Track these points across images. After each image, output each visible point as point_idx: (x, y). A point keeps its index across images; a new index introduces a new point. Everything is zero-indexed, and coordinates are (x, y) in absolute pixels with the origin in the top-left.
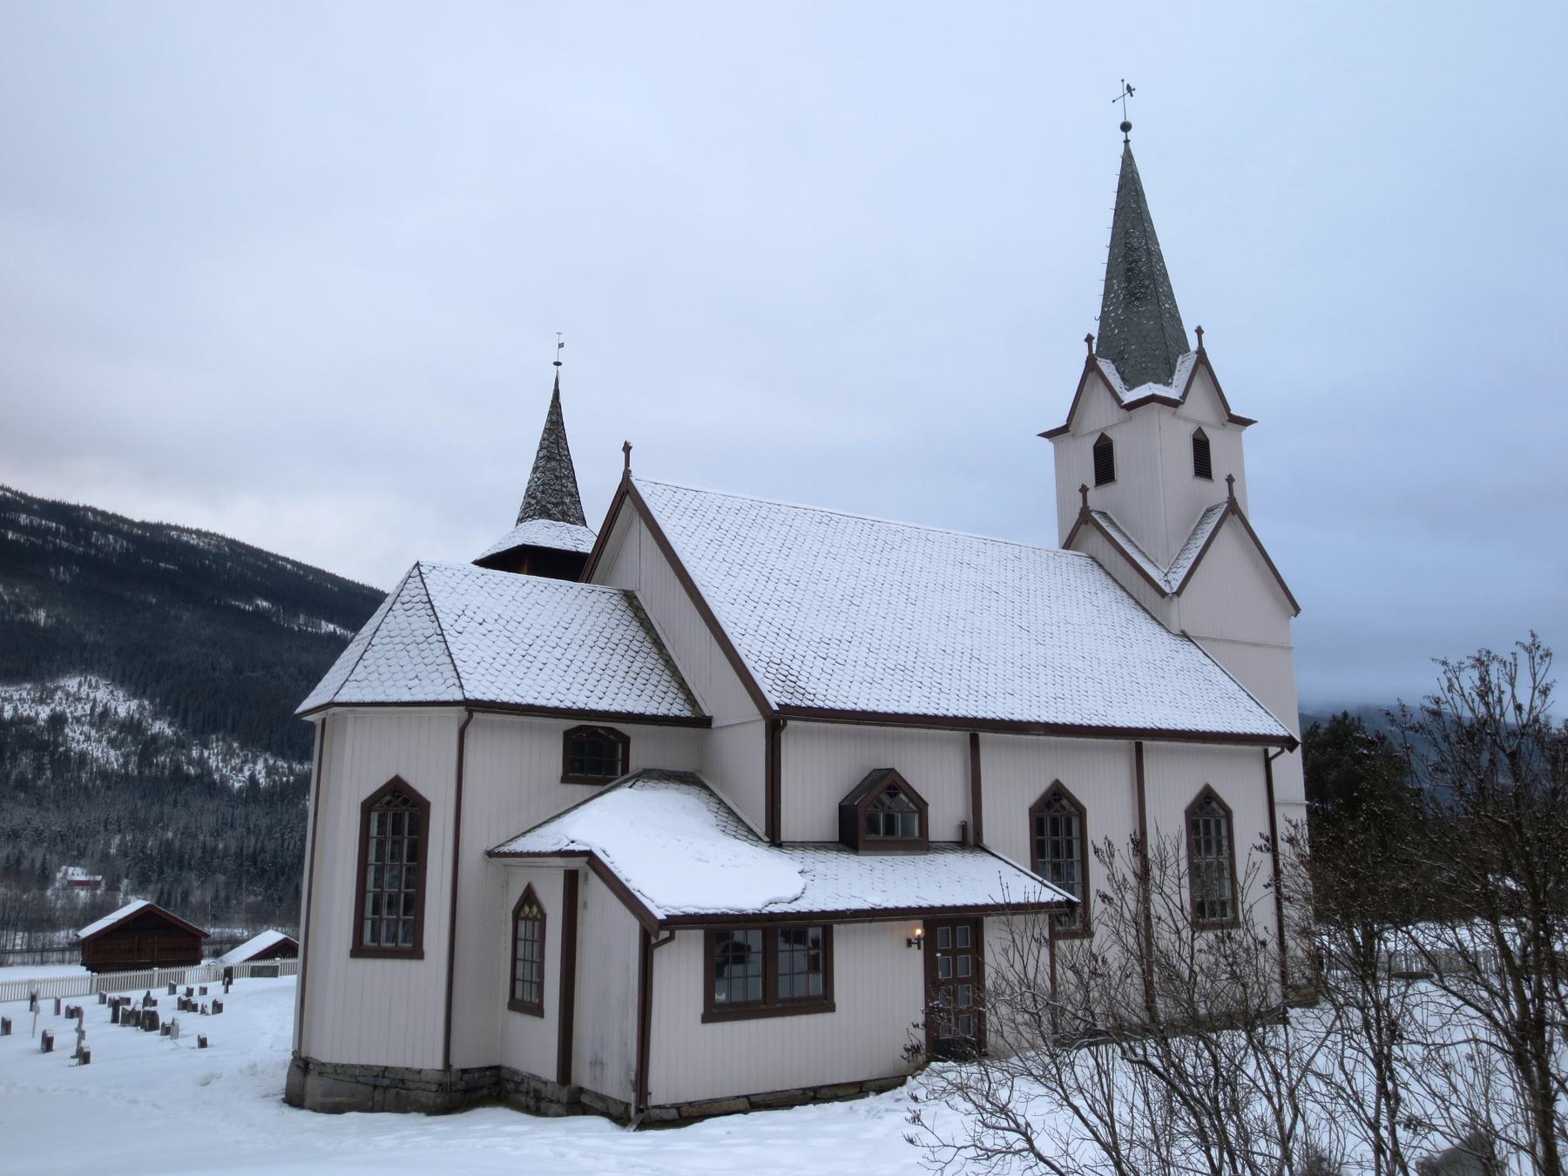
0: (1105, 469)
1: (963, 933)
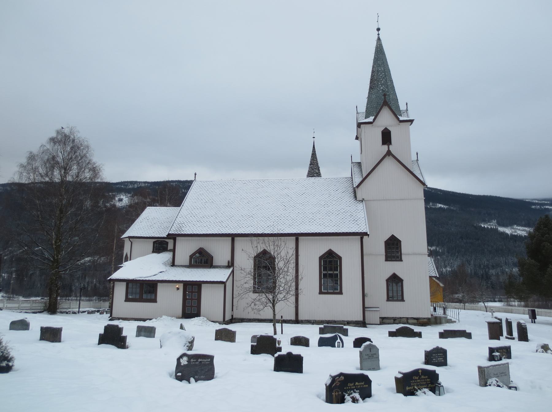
0: (386, 137)
1: (195, 288)
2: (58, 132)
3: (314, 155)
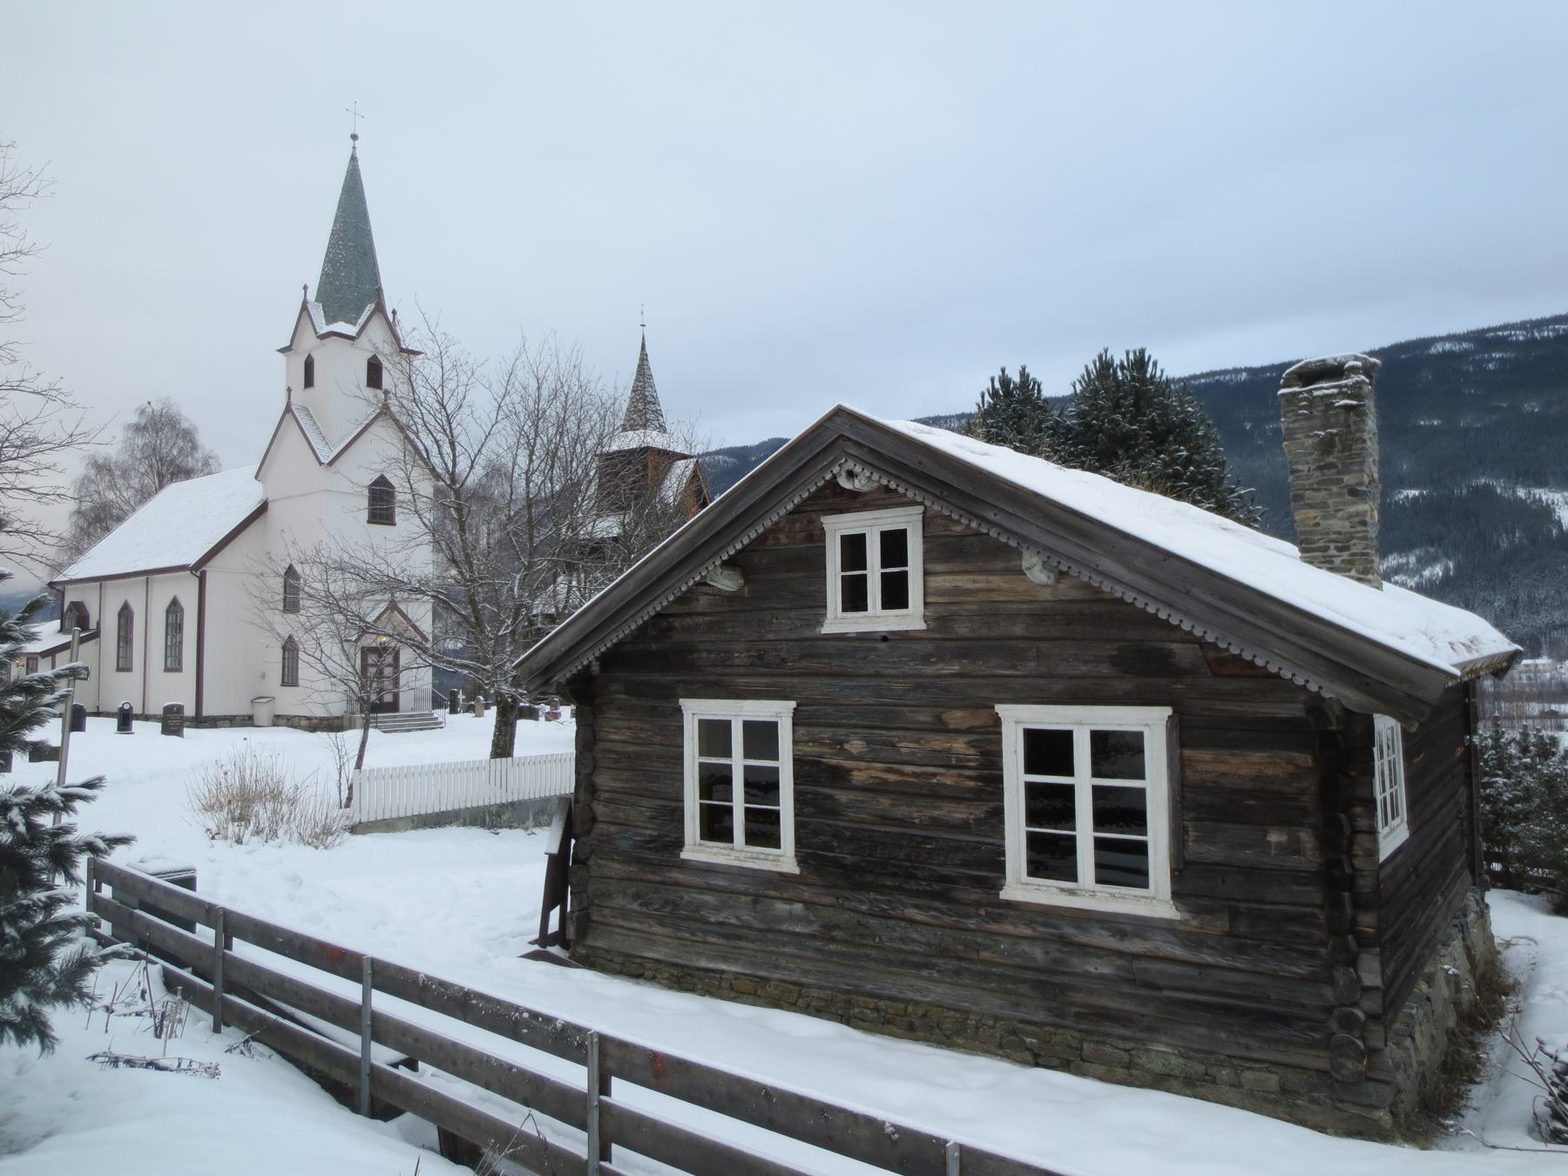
2: (143, 412)
3: (644, 358)
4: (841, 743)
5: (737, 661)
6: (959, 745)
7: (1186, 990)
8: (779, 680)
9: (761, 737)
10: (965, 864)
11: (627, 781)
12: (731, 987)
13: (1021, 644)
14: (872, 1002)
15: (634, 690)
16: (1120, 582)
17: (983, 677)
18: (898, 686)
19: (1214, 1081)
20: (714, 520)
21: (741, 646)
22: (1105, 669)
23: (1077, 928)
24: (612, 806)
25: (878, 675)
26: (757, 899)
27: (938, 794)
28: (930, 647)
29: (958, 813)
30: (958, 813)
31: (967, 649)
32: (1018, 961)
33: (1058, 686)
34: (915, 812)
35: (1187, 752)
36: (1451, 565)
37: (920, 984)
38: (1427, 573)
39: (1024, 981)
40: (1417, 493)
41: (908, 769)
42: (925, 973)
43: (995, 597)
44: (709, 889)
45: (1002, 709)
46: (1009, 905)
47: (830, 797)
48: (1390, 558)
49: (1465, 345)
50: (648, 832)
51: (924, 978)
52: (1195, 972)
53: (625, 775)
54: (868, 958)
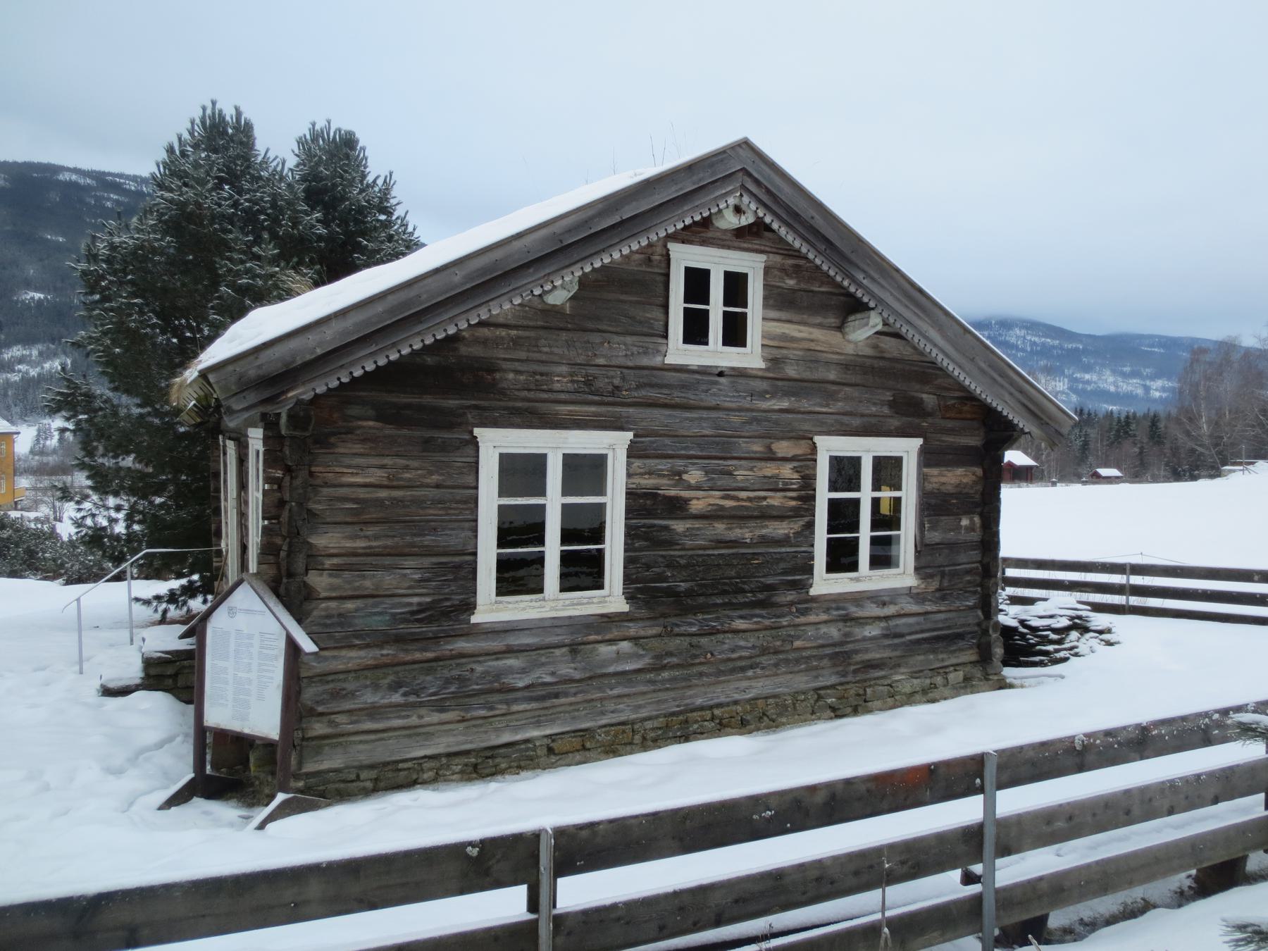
4: (680, 474)
5: (557, 386)
6: (787, 471)
7: (917, 633)
8: (610, 409)
9: (583, 472)
10: (785, 573)
11: (376, 538)
12: (550, 751)
13: (835, 388)
14: (708, 714)
15: (389, 416)
16: (935, 345)
17: (803, 413)
18: (735, 419)
19: (936, 687)
20: (592, 218)
21: (564, 369)
22: (886, 410)
23: (857, 606)
24: (347, 574)
25: (716, 408)
26: (574, 649)
27: (766, 515)
28: (764, 385)
29: (780, 529)
30: (780, 529)
31: (798, 388)
32: (820, 642)
33: (856, 422)
34: (745, 533)
35: (925, 470)
36: (69, 362)
37: (745, 684)
38: (47, 366)
39: (821, 658)
40: (42, 296)
41: (743, 494)
42: (750, 673)
43: (812, 346)
44: (510, 651)
45: (819, 440)
46: (815, 599)
47: (666, 528)
48: (15, 349)
49: (89, 181)
50: (415, 600)
51: (749, 678)
52: (921, 619)
53: (371, 530)
54: (701, 674)
